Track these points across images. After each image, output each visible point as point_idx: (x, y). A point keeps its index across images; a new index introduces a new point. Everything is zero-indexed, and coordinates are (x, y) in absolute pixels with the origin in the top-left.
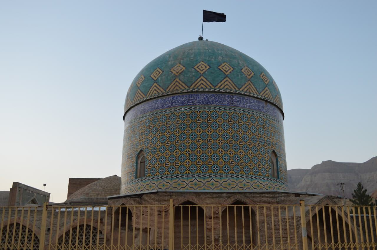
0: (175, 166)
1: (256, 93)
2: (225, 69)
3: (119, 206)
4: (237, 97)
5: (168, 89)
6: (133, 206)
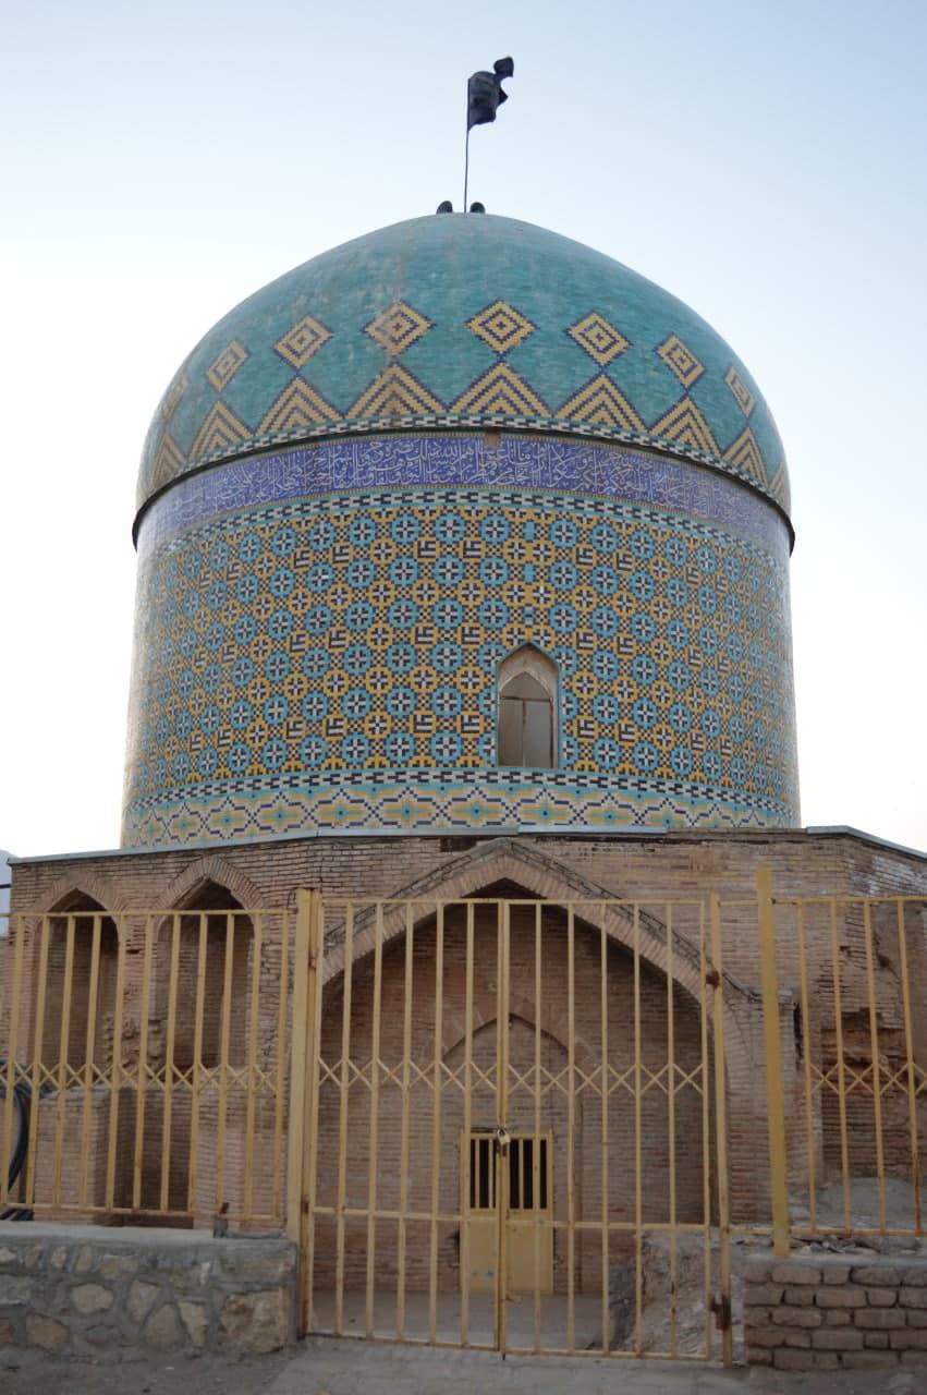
0: (416, 731)
1: (710, 449)
2: (595, 341)
3: (170, 912)
4: (337, 451)
5: (358, 407)
6: (341, 902)
